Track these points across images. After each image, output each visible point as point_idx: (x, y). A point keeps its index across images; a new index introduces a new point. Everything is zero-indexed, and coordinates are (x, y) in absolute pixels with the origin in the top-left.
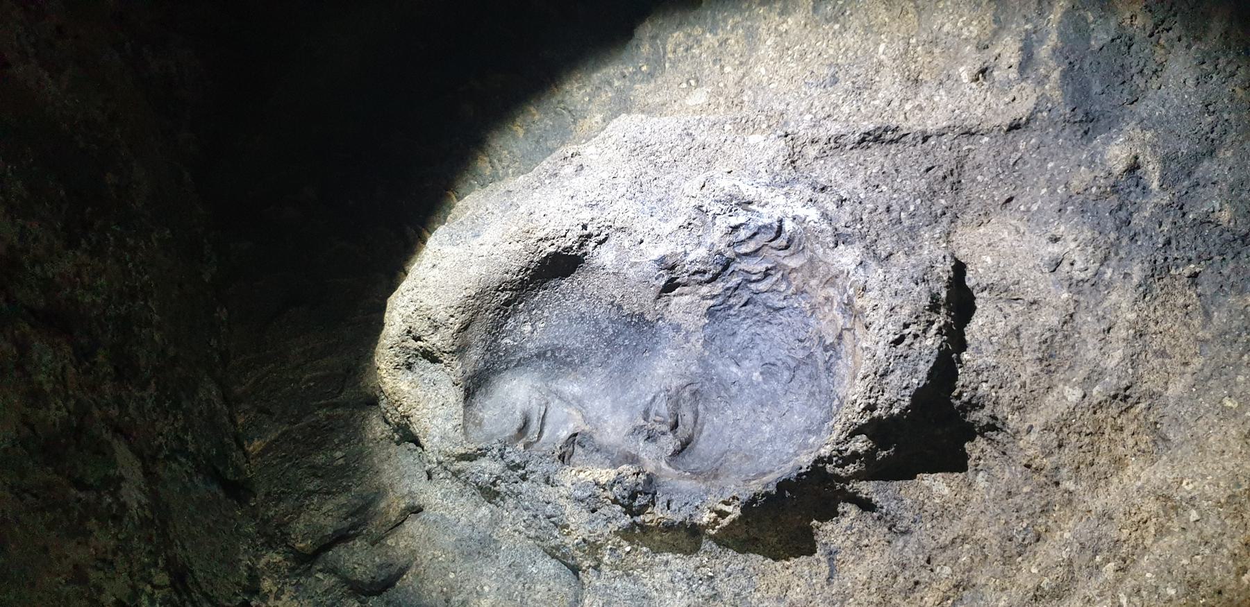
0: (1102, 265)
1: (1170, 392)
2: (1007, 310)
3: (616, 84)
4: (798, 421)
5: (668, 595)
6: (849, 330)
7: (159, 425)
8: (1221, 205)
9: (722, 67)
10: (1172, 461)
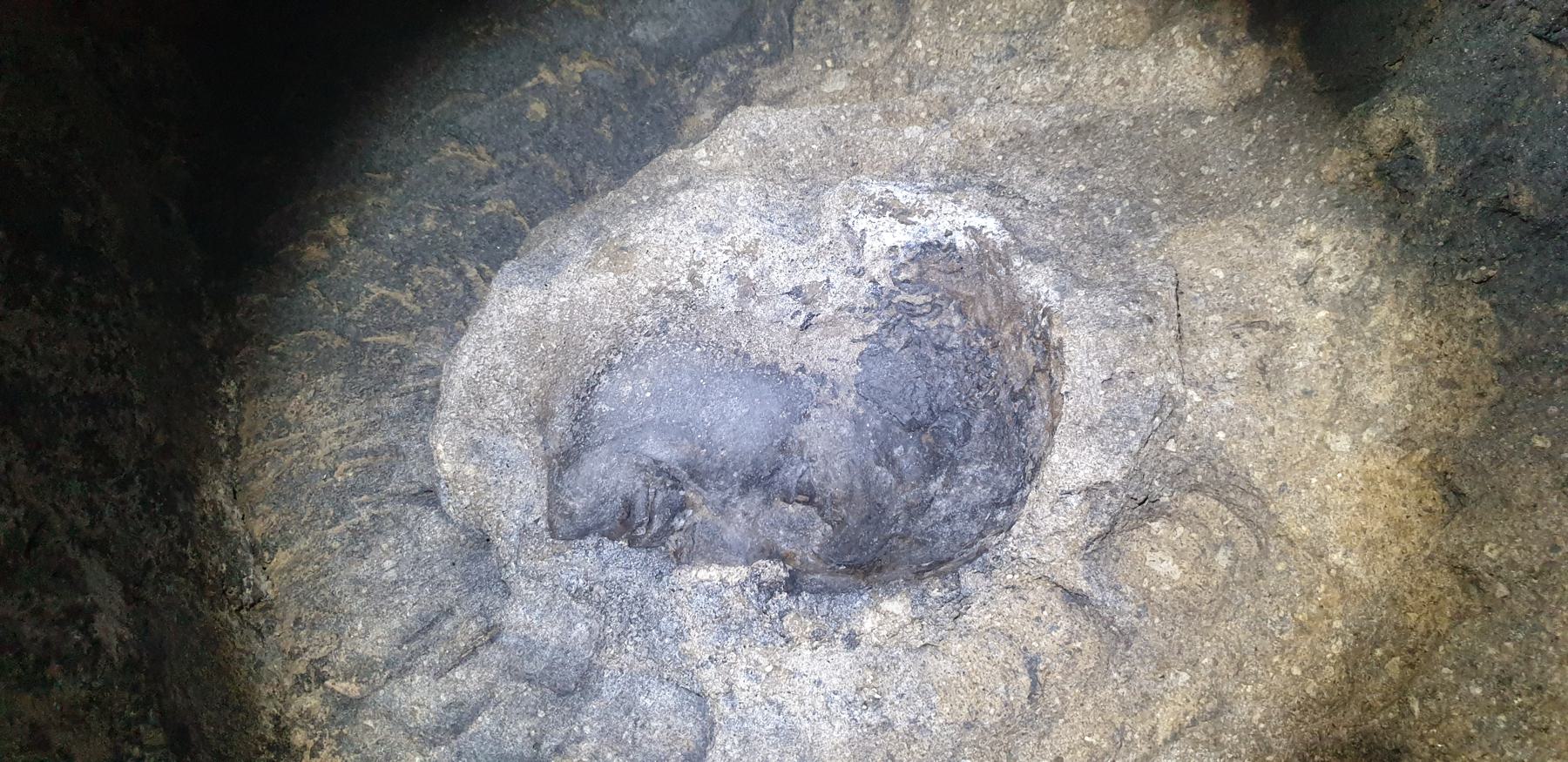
0: (1366, 273)
1: (1461, 432)
2: (1246, 336)
3: (731, 68)
4: (981, 493)
5: (824, 726)
6: (1043, 371)
7: (147, 536)
8: (1516, 187)
9: (866, 42)
10: (1468, 521)
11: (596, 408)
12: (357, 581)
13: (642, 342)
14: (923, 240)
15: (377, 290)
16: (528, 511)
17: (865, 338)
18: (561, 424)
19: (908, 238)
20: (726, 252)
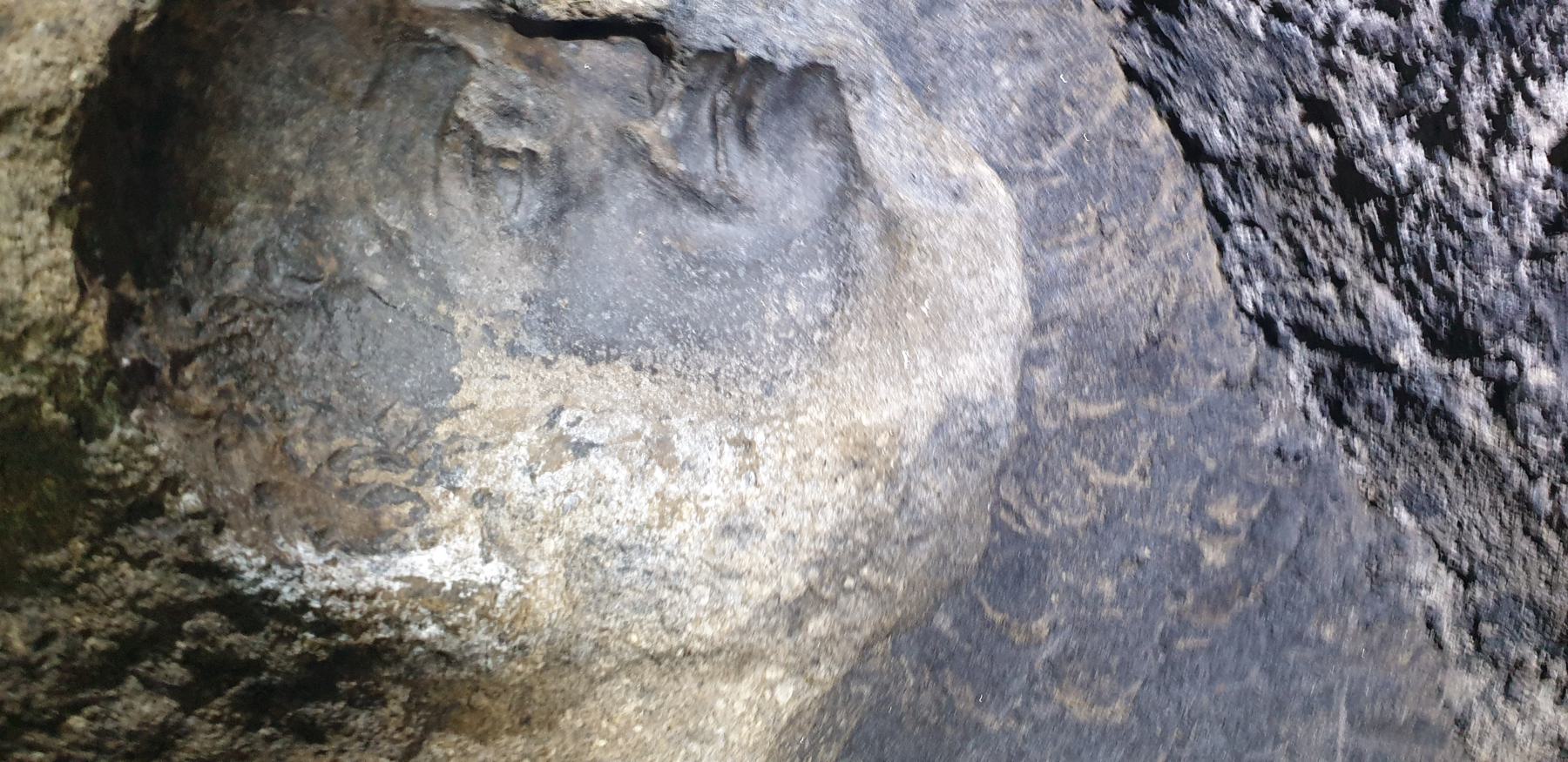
11: (826, 269)
12: (1034, 54)
13: (792, 364)
14: (377, 558)
15: (1131, 478)
16: (872, 115)
17: (455, 413)
18: (866, 232)
19: (406, 560)
20: (707, 498)
